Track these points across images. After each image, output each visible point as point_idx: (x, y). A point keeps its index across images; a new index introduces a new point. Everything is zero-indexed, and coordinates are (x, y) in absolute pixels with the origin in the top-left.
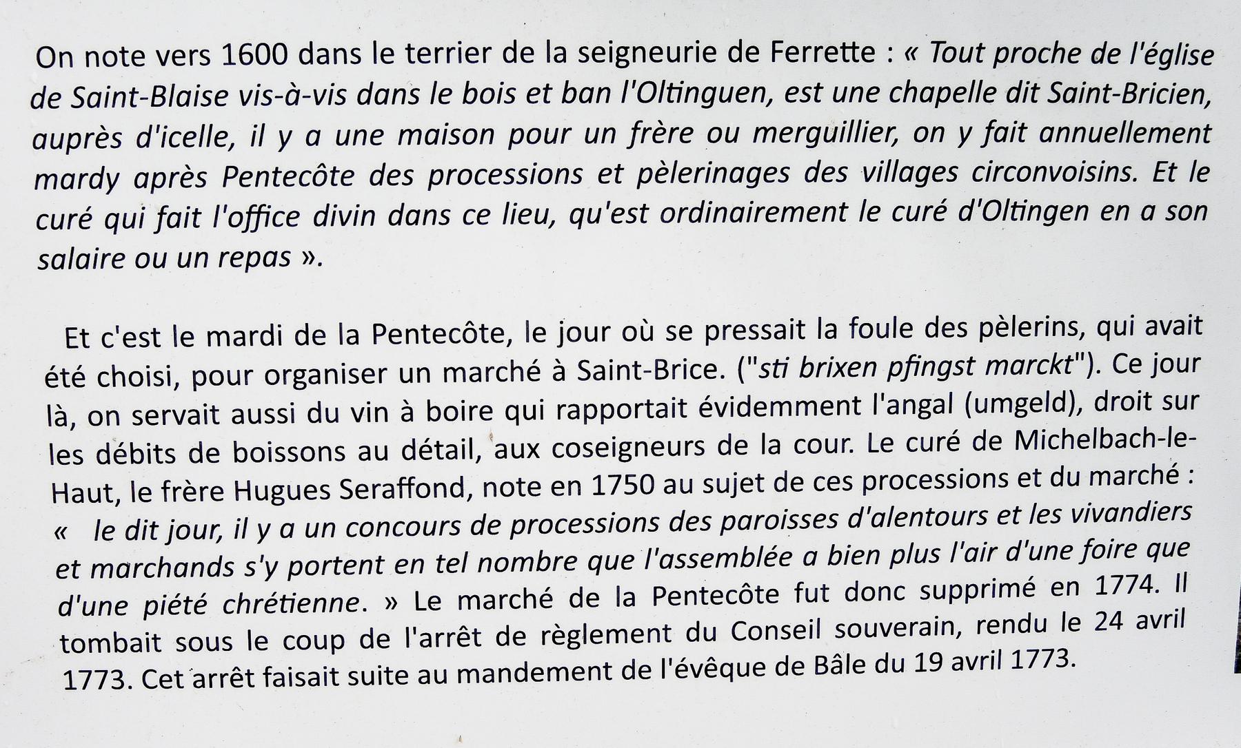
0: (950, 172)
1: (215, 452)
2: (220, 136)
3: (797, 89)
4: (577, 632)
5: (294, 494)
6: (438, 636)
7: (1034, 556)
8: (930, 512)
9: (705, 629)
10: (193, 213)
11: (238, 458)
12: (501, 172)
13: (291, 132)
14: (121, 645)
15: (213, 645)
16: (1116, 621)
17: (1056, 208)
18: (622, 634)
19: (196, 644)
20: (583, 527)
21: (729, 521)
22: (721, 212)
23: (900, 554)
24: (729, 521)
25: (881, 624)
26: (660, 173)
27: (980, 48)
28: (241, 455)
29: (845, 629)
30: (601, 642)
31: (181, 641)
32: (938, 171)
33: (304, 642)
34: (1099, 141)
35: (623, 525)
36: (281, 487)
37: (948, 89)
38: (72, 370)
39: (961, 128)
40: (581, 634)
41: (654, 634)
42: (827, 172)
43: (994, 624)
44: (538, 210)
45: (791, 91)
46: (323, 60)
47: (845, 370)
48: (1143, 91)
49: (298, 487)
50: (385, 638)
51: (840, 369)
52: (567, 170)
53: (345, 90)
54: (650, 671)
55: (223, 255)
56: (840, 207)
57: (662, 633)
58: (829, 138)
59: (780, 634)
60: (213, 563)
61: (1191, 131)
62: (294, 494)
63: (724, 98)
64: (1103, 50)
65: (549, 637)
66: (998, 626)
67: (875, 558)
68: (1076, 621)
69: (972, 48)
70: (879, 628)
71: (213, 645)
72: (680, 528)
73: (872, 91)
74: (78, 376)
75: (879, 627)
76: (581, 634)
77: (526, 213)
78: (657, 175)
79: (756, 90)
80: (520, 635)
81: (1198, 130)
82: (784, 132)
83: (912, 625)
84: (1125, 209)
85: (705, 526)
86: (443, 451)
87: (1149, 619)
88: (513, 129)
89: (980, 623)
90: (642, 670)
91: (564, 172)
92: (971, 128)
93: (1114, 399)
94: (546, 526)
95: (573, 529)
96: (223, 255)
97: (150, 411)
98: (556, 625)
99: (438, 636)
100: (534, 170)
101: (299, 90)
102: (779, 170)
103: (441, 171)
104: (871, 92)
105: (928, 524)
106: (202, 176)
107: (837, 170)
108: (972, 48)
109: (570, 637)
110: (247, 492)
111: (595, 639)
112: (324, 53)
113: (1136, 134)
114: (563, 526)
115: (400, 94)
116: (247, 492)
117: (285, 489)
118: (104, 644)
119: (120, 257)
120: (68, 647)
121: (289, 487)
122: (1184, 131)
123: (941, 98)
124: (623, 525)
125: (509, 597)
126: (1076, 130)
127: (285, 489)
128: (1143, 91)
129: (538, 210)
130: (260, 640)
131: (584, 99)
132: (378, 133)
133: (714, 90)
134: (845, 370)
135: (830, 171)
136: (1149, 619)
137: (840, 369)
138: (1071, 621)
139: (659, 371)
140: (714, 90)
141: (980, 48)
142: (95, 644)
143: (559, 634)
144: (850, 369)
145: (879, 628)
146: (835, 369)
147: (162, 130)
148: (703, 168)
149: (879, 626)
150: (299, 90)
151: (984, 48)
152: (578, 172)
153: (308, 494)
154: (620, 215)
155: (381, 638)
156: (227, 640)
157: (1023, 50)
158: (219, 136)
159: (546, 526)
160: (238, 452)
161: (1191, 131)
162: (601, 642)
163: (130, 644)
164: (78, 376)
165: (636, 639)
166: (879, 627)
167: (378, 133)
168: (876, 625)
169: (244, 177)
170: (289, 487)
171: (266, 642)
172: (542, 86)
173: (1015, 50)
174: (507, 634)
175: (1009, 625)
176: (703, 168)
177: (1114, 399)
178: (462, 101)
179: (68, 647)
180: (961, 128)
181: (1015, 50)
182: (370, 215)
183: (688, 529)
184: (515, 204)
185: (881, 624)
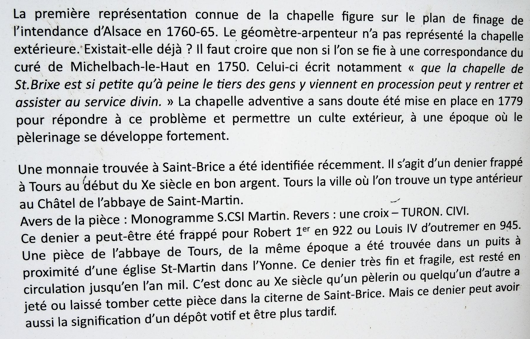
0: (262, 84)
1: (87, 13)
2: (209, 84)
3: (259, 83)
4: (135, 268)
5: (359, 18)
7: (371, 84)
8: (493, 83)
10: (123, 82)
11: (332, 247)
12: (70, 84)
13: (305, 82)
17: (275, 83)
20: (408, 86)
21: (442, 85)
22: (189, 84)
23: (442, 84)
24: (442, 85)
26: (279, 84)
27: (460, 83)
28: (218, 184)
30: (281, 252)
32: (209, 84)
34: (430, 83)
35: (425, 85)
36: (354, 15)
37: (172, 82)
38: (395, 98)
39: (311, 82)
40: (137, 269)
42: (342, 84)
44: (453, 83)
45: (67, 84)
47: (52, 86)
48: (41, 83)
49: (79, 292)
51: (50, 85)
52: (289, 83)
53: (264, 82)
54: (299, 249)
55: (476, 84)
56: (354, 82)
58: (329, 84)
61: (487, 84)
62: (359, 18)
63: (329, 84)
64: (252, 83)
67: (330, 85)
69: (457, 83)
72: (251, 87)
73: (195, 84)
74: (460, 35)
76: (137, 269)
77: (343, 84)
78: (176, 85)
79: (369, 83)
81: (351, 83)
82: (404, 84)
84: (432, 84)
85: (262, 86)
88: (169, 82)
90: (380, 245)
91: (287, 83)
92: (305, 82)
94: (393, 85)
95: (404, 87)
96: (476, 84)
97: (152, 267)
98: (371, 273)
100: (420, 83)
101: (162, 82)
102: (260, 83)
103: (383, 83)
104: (129, 84)
105: (124, 88)
106: (263, 83)
107: (260, 83)
108: (457, 83)
110: (163, 65)
111: (183, 320)
113: (208, 85)
114: (400, 85)
115: (287, 84)
116: (163, 65)
117: (355, 16)
119: (57, 84)
121: (357, 15)
122: (484, 84)
123: (251, 84)
124: (425, 85)
125: (38, 288)
126: (334, 83)
127: (355, 16)
128: (41, 83)
129: (453, 83)
131: (171, 83)
132: (196, 83)
133: (144, 83)
134: (52, 86)
135: (257, 83)
137: (50, 85)
139: (33, 85)
140: (144, 83)
141: (460, 83)
144: (55, 85)
146: (48, 85)
148: (43, 83)
150: (162, 82)
151: (462, 83)
152: (293, 83)
153: (69, 239)
154: (131, 85)
157: (390, 83)
158: (209, 84)
159: (393, 85)
160: (101, 186)
161: (487, 84)
162: (281, 252)
164: (171, 235)
167: (196, 83)
169: (209, 84)
170: (357, 15)
172: (519, 82)
173: (387, 83)
176: (43, 83)
178: (163, 83)
180: (311, 82)
181: (387, 83)
182: (371, 84)
183: (278, 87)
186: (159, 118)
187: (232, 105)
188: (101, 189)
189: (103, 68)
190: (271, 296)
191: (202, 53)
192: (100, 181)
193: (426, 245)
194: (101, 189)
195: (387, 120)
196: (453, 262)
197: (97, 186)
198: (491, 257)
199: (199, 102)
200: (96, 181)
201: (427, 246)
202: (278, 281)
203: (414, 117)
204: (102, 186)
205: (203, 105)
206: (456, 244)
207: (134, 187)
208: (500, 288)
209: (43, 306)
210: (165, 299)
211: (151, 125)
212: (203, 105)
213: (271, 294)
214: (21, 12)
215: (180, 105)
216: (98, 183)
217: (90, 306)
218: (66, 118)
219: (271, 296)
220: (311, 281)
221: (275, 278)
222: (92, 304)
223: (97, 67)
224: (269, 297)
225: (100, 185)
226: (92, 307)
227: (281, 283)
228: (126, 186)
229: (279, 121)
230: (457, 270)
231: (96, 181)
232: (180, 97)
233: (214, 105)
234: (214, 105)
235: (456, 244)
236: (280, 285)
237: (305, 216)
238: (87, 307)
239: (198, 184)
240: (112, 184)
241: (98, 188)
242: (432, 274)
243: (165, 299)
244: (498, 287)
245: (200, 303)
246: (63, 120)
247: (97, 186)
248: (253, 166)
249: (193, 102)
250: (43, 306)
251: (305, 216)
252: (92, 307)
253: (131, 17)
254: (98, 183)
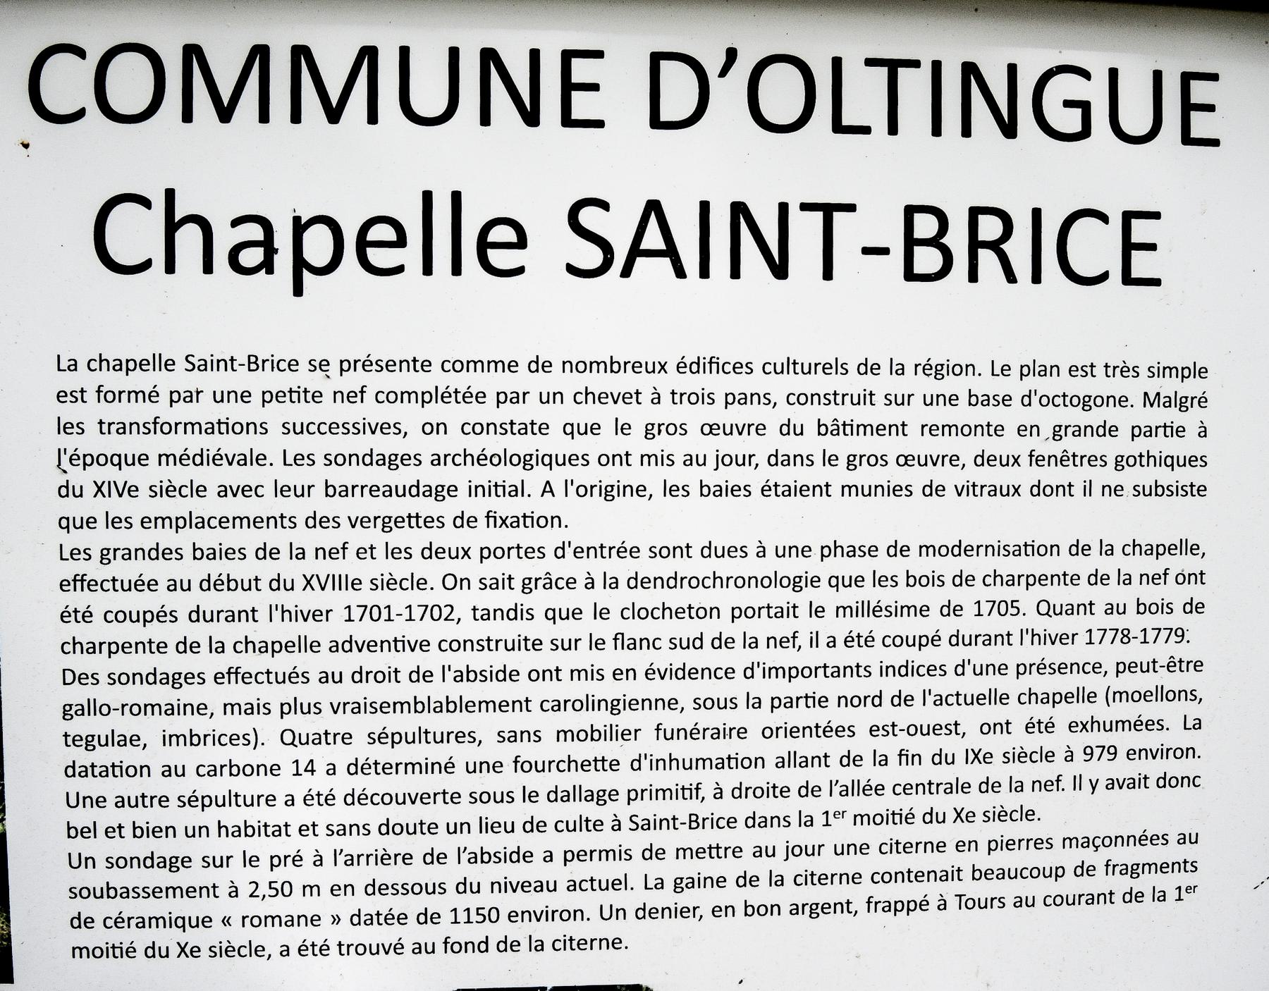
6: (353, 487)
9: (937, 813)
14: (112, 893)
15: (499, 799)
16: (309, 768)
18: (178, 891)
19: (485, 798)
25: (931, 456)
29: (701, 702)
31: (697, 701)
33: (387, 799)
41: (807, 731)
43: (920, 874)
46: (785, 463)
50: (317, 918)
57: (671, 822)
59: (823, 400)
60: (739, 877)
65: (920, 369)
66: (923, 876)
68: (1093, 695)
70: (381, 948)
71: (430, 890)
75: (734, 427)
80: (261, 457)
83: (705, 730)
86: (780, 490)
87: (228, 489)
89: (923, 427)
93: (747, 789)
99: (353, 487)
109: (937, 370)
112: (786, 458)
118: (406, 706)
120: (70, 742)
130: (253, 859)
136: (228, 489)
138: (937, 487)
142: (406, 396)
143: (230, 949)
145: (381, 948)
147: (761, 666)
149: (407, 796)
155: (332, 551)
156: (530, 611)
163: (338, 490)
165: (784, 645)
166: (734, 427)
168: (732, 425)
171: (275, 800)
174: (353, 796)
175: (706, 672)
177: (747, 789)
179: (70, 742)
184: (764, 664)
185: (931, 456)
186: (865, 698)
187: (154, 370)
188: (229, 589)
189: (677, 613)
190: (806, 875)
191: (817, 647)
192: (228, 575)
193: (837, 731)
194: (229, 589)
195: (981, 702)
196: (1204, 554)
197: (223, 584)
198: (885, 728)
199: (94, 365)
200: (221, 574)
201: (151, 587)
202: (959, 815)
203: (1069, 754)
204: (233, 585)
205: (101, 370)
206: (259, 429)
207: (289, 586)
208: (1113, 784)
209: (296, 858)
210: (706, 847)
211: (481, 562)
212: (101, 370)
213: (806, 871)
214: (69, 360)
215: (59, 370)
216: (224, 578)
217: (142, 894)
218: (85, 456)
219: (806, 875)
220: (1016, 816)
221: (955, 809)
222: (146, 890)
223: (667, 612)
224: (560, 941)
225: (229, 581)
226: (147, 895)
227: (964, 819)
228: (275, 585)
229: (608, 556)
230: (722, 59)
231: (221, 574)
232: (59, 356)
233: (121, 369)
234: (121, 369)
235: (259, 429)
236: (963, 822)
237: (654, 673)
238: (136, 895)
239: (145, 520)
240: (250, 580)
241: (225, 587)
242: (1116, 846)
243: (706, 847)
244: (1111, 782)
245: (229, 953)
246: (79, 459)
247: (223, 584)
248: (1021, 755)
249: (82, 365)
250: (296, 858)
251: (654, 673)
252: (147, 895)
253: (340, 433)
254: (224, 578)
